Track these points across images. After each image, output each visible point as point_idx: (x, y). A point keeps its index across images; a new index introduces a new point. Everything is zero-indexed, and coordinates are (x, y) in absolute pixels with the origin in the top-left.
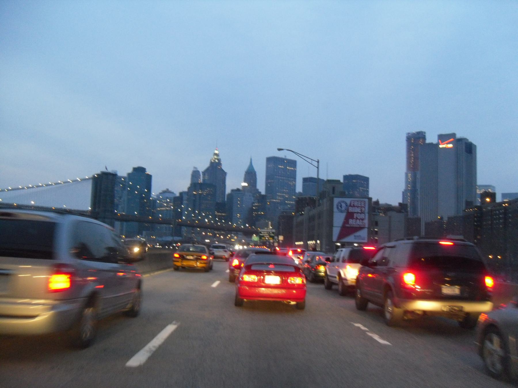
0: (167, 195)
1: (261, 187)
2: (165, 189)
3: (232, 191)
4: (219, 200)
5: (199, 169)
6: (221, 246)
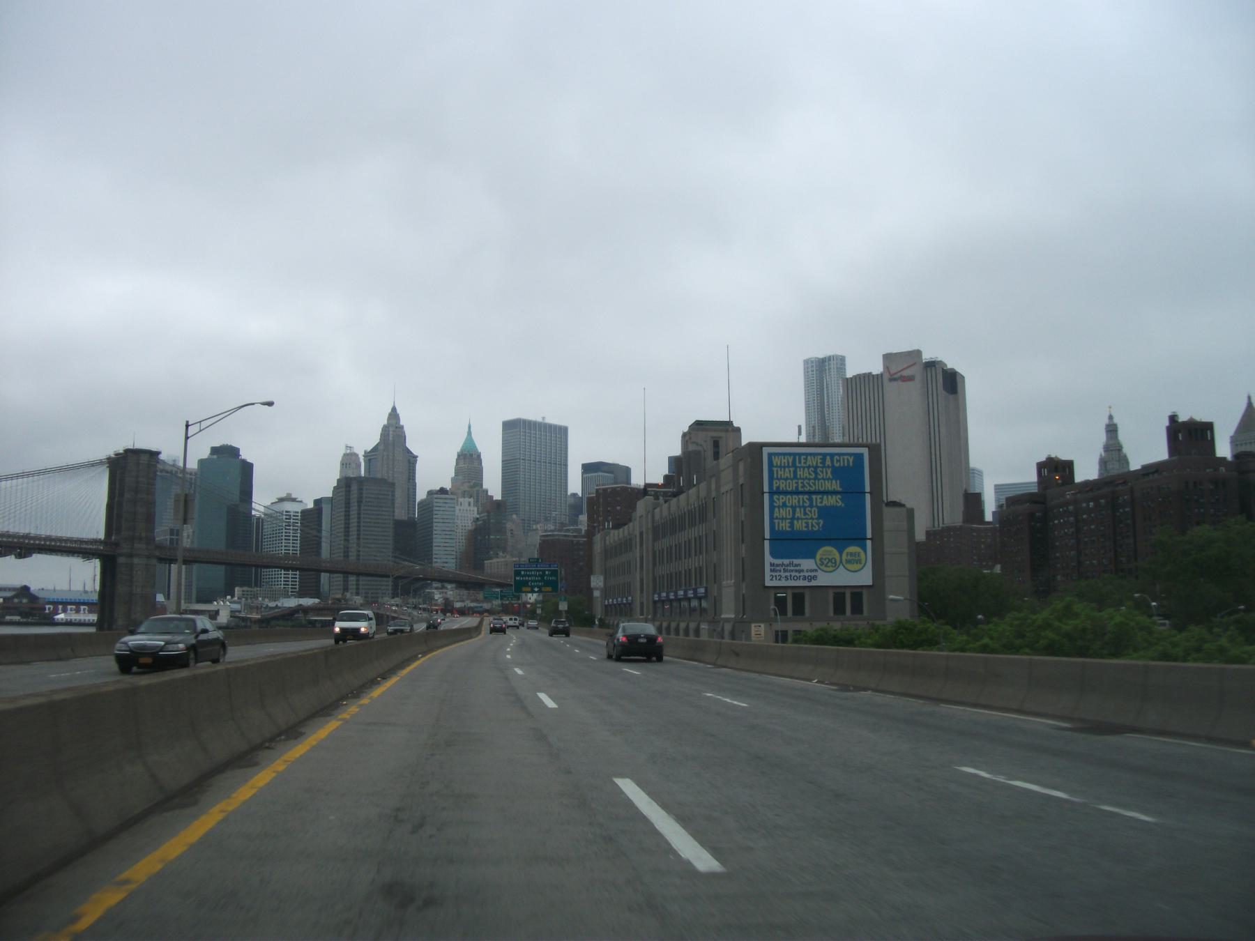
0: (288, 506)
1: (493, 483)
2: (284, 495)
3: (430, 493)
4: (400, 514)
5: (356, 451)
6: (470, 608)
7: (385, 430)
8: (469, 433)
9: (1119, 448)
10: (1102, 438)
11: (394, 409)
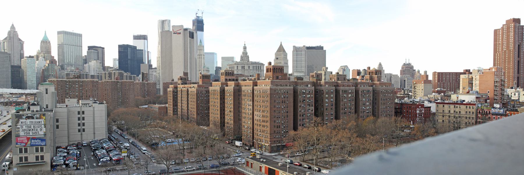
1: (55, 53)
7: (9, 33)
8: (45, 34)
9: (247, 54)
10: (242, 50)
11: (13, 25)
